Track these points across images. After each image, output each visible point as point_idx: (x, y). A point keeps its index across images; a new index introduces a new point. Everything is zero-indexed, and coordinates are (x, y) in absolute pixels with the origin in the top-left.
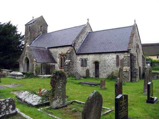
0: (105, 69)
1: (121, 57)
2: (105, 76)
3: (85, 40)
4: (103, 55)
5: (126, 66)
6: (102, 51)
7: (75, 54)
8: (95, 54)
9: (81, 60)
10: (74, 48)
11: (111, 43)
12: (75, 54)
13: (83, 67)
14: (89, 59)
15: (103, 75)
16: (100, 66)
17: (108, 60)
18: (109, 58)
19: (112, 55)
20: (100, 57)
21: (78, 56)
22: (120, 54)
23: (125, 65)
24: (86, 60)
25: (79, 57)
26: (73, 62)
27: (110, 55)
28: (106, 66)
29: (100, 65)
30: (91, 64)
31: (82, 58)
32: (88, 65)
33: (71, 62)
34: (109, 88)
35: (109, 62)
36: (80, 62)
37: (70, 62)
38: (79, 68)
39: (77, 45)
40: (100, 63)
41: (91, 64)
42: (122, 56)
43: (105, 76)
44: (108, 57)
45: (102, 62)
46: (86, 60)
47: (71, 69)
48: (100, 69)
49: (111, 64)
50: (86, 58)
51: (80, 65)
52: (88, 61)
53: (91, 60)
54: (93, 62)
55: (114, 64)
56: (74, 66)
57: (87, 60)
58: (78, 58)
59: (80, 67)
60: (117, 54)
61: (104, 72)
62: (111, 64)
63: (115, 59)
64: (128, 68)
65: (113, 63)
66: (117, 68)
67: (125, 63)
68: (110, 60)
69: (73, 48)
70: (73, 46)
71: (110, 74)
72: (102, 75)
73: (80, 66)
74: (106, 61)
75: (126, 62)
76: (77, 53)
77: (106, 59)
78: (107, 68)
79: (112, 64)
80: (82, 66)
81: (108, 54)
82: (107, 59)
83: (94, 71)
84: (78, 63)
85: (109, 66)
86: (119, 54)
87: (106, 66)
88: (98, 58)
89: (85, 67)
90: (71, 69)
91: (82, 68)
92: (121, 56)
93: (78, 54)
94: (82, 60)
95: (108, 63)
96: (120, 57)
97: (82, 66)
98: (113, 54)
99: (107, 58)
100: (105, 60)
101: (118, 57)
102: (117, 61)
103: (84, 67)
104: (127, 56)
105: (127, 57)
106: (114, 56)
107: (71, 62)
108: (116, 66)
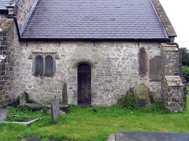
0: (110, 82)
1: (151, 52)
2: (109, 99)
3: (36, 8)
4: (104, 46)
5: (170, 74)
6: (101, 35)
7: (16, 39)
8: (80, 44)
9: (34, 57)
10: (15, 21)
11: (114, 19)
12: (17, 39)
13: (42, 78)
14: (63, 56)
15: (104, 98)
16: (96, 73)
17: (118, 59)
18: (120, 54)
19: (127, 46)
20: (94, 50)
21: (24, 47)
22: (150, 46)
23: (168, 71)
24: (50, 58)
25: (28, 50)
26: (13, 64)
27: (122, 47)
28: (111, 75)
29: (94, 72)
30: (69, 69)
31: (39, 51)
32: (59, 72)
33: (7, 63)
34: (142, 129)
35: (121, 64)
36: (31, 63)
37: (5, 61)
38: (27, 79)
39: (22, 15)
40: (96, 65)
41: (69, 69)
42: (153, 51)
43: (109, 99)
44: (118, 52)
45: (99, 64)
46: (50, 58)
47: (9, 84)
48: (93, 83)
49: (125, 69)
50: (51, 51)
51: (31, 70)
52: (57, 62)
53: (67, 58)
54: (74, 62)
55: (133, 68)
56: (15, 73)
57: (54, 56)
58: (24, 51)
59: (33, 77)
60: (141, 45)
61: (106, 90)
62: (125, 69)
63: (137, 58)
64: (176, 78)
65: (131, 67)
66: (141, 80)
67: (168, 68)
68: (123, 59)
69: (12, 20)
70: (10, 13)
71: (124, 93)
72: (101, 98)
73: (30, 74)
74: (113, 62)
75: (171, 65)
76: (24, 37)
77: (112, 57)
78: (116, 79)
79: (128, 70)
80: (36, 74)
81: (117, 44)
82: (116, 56)
83: (75, 88)
84: (24, 64)
85: (119, 74)
86: (146, 46)
87: (111, 75)
88: (89, 53)
89: (48, 76)
90: (9, 84)
91: (39, 78)
92: (151, 50)
93: (24, 41)
94: (39, 58)
95: (117, 66)
96: (147, 51)
97: (37, 73)
98: (131, 45)
99: (114, 55)
100: (109, 60)
101: (142, 52)
102: (140, 62)
103: (46, 78)
104: (173, 51)
105: (174, 53)
106: (134, 49)
107: (7, 63)
108: (138, 73)
